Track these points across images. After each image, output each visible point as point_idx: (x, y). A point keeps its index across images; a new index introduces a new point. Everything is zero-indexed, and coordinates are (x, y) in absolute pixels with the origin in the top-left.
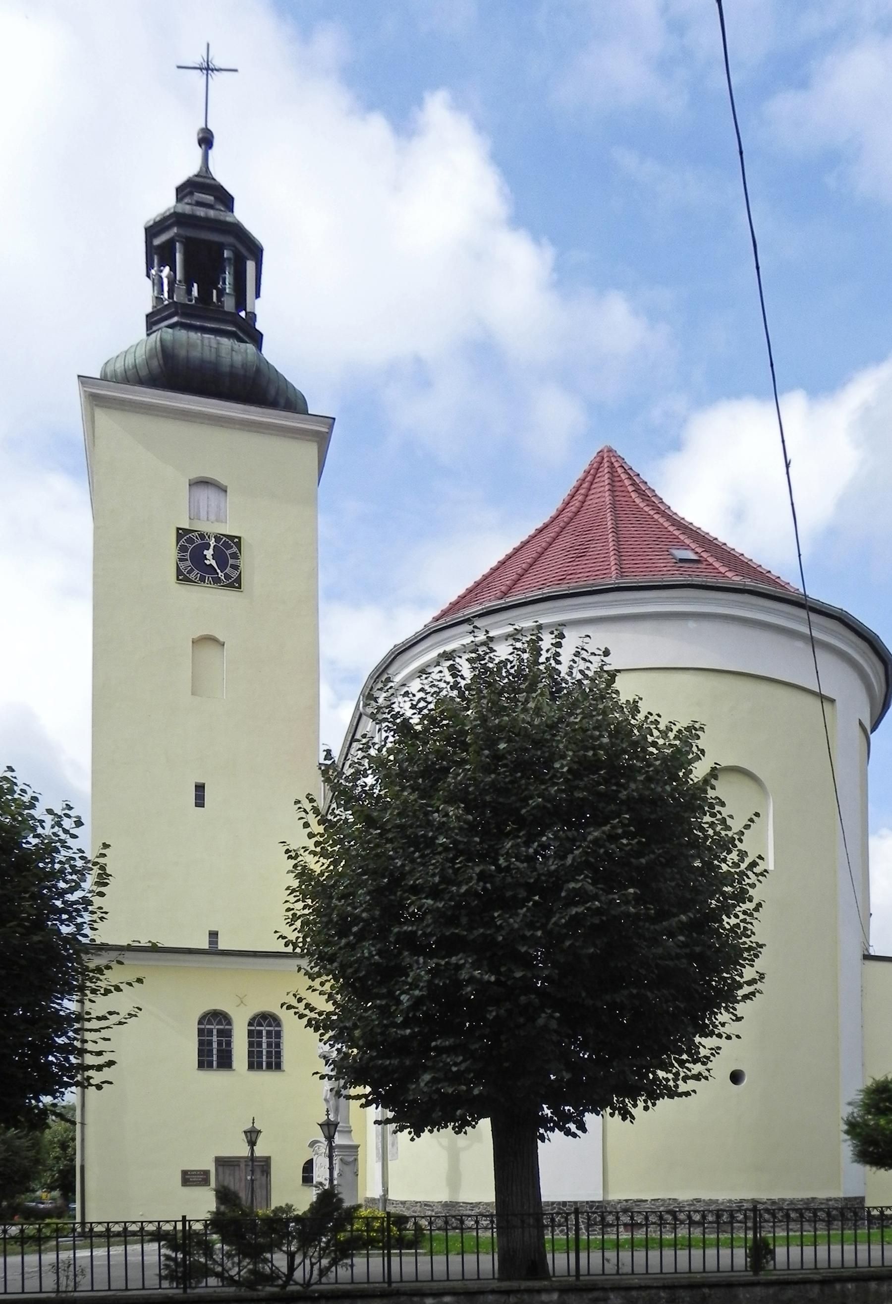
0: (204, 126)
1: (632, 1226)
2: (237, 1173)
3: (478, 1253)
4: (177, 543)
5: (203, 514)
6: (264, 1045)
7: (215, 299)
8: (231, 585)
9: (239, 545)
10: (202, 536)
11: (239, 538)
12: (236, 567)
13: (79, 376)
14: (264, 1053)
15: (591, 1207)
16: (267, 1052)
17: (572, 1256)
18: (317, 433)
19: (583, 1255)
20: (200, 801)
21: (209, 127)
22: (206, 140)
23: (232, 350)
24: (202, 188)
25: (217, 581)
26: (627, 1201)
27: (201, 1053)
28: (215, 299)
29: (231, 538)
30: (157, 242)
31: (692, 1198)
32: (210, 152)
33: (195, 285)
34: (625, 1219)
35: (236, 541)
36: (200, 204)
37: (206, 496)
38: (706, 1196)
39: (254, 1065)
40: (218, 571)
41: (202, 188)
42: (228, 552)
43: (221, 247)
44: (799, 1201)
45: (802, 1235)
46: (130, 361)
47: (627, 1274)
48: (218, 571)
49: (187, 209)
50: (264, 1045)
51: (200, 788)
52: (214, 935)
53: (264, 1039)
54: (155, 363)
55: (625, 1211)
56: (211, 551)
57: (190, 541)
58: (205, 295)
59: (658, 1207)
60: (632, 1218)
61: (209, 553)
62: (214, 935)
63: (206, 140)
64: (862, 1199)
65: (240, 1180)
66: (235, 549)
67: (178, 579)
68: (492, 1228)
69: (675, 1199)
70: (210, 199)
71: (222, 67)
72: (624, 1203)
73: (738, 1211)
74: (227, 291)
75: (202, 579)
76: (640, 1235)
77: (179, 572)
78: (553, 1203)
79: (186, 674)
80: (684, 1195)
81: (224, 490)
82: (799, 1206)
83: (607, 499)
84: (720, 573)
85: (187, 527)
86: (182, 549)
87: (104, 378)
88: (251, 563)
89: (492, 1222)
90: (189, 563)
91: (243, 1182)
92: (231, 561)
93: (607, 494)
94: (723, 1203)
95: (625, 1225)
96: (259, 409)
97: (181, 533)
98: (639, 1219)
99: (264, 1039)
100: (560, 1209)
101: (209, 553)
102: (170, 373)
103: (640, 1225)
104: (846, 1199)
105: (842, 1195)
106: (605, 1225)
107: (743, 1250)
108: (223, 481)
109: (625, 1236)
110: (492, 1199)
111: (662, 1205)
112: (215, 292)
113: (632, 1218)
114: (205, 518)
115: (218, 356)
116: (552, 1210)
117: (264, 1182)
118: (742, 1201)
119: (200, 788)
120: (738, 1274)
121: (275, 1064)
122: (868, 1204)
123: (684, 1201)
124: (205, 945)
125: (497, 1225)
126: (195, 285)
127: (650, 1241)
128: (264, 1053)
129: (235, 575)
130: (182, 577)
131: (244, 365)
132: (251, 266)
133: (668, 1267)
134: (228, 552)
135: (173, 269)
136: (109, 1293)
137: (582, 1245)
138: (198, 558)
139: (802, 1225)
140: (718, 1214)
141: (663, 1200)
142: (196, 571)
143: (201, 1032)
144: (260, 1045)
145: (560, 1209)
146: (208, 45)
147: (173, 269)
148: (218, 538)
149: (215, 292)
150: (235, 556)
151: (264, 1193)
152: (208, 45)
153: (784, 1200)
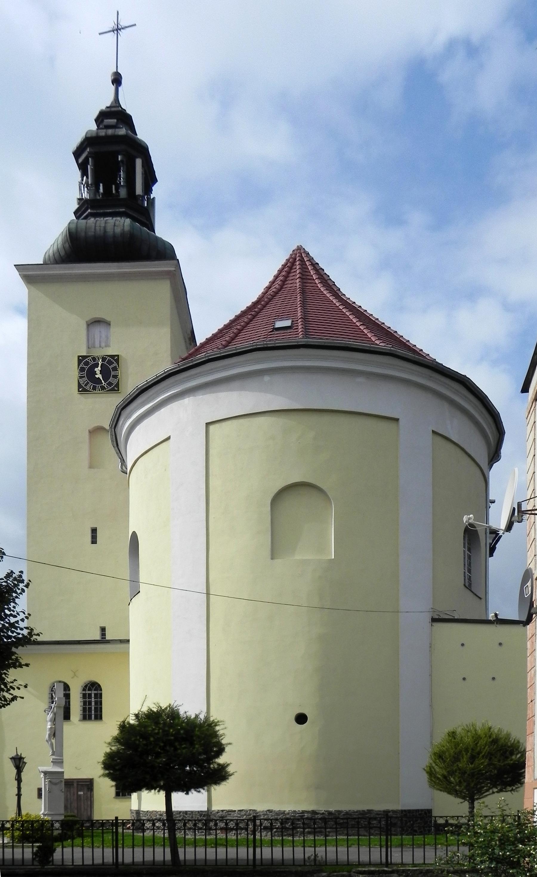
0: (115, 70)
1: (226, 830)
2: (72, 789)
3: (304, 847)
4: (79, 365)
5: (97, 344)
6: (93, 704)
7: (114, 192)
8: (113, 390)
9: (117, 361)
10: (94, 359)
11: (118, 356)
12: (115, 377)
13: (15, 265)
14: (93, 708)
15: (201, 815)
16: (95, 708)
17: (251, 850)
18: (168, 273)
19: (258, 850)
20: (94, 541)
21: (119, 71)
22: (117, 80)
23: (115, 225)
24: (115, 116)
25: (103, 388)
26: (222, 811)
27: (84, 710)
28: (114, 192)
29: (112, 356)
30: (80, 161)
31: (266, 810)
32: (120, 89)
33: (101, 185)
34: (222, 825)
35: (116, 358)
36: (107, 127)
37: (98, 331)
38: (276, 808)
39: (86, 716)
40: (103, 381)
41: (115, 116)
42: (111, 367)
43: (115, 154)
44: (354, 812)
45: (358, 838)
46: (55, 247)
47: (300, 866)
48: (103, 381)
49: (102, 133)
50: (93, 704)
51: (94, 531)
52: (103, 630)
53: (93, 700)
54: (67, 245)
55: (222, 819)
56: (99, 368)
57: (87, 363)
58: (107, 190)
59: (243, 816)
60: (227, 824)
61: (98, 370)
62: (103, 630)
63: (117, 80)
64: (430, 811)
65: (74, 795)
66: (115, 364)
67: (79, 391)
68: (164, 830)
69: (254, 810)
70: (113, 121)
71: (127, 25)
72: (221, 813)
73: (298, 820)
74: (122, 184)
75: (94, 388)
76: (232, 836)
77: (80, 386)
78: (180, 812)
79: (84, 454)
80: (260, 807)
81: (108, 324)
82: (355, 816)
83: (298, 284)
84: (357, 326)
85: (85, 354)
86: (82, 370)
87: (45, 263)
88: (73, 373)
89: (164, 825)
90: (86, 379)
91: (76, 795)
92: (113, 373)
93: (298, 281)
94: (288, 814)
95: (221, 829)
96: (127, 264)
97: (81, 359)
98: (232, 825)
99: (93, 700)
100: (184, 816)
101: (98, 370)
102: (80, 249)
103: (232, 829)
104: (402, 811)
105: (400, 808)
106: (208, 829)
107: (31, 850)
108: (108, 319)
109: (221, 835)
110: (165, 810)
111: (245, 815)
112: (114, 186)
113: (227, 824)
114: (99, 346)
115: (105, 231)
116: (180, 817)
117: (89, 796)
118: (303, 812)
119: (94, 531)
120: (17, 867)
121: (101, 718)
122: (434, 814)
123: (260, 812)
124: (98, 637)
125: (168, 827)
126: (101, 185)
127: (273, 841)
128: (93, 708)
129: (115, 382)
130: (82, 389)
131: (123, 234)
132: (139, 162)
133: (98, 861)
134: (111, 367)
135: (87, 177)
136: (144, 867)
137: (258, 843)
138: (91, 374)
139: (358, 831)
140: (283, 822)
141: (247, 811)
142: (90, 383)
143: (84, 696)
144: (90, 703)
145: (184, 816)
146: (118, 12)
147: (87, 177)
148: (104, 359)
149: (114, 186)
150: (115, 369)
151: (89, 803)
152: (118, 12)
153: (339, 812)
